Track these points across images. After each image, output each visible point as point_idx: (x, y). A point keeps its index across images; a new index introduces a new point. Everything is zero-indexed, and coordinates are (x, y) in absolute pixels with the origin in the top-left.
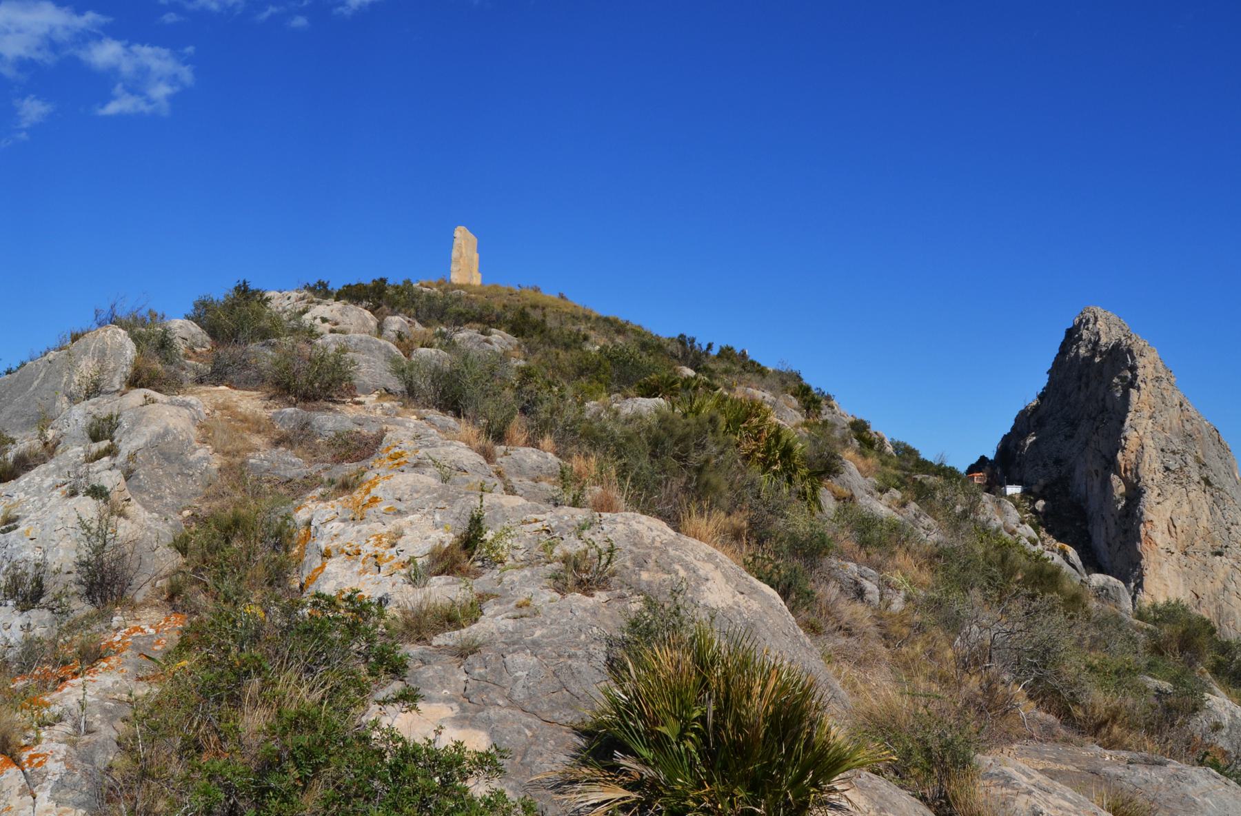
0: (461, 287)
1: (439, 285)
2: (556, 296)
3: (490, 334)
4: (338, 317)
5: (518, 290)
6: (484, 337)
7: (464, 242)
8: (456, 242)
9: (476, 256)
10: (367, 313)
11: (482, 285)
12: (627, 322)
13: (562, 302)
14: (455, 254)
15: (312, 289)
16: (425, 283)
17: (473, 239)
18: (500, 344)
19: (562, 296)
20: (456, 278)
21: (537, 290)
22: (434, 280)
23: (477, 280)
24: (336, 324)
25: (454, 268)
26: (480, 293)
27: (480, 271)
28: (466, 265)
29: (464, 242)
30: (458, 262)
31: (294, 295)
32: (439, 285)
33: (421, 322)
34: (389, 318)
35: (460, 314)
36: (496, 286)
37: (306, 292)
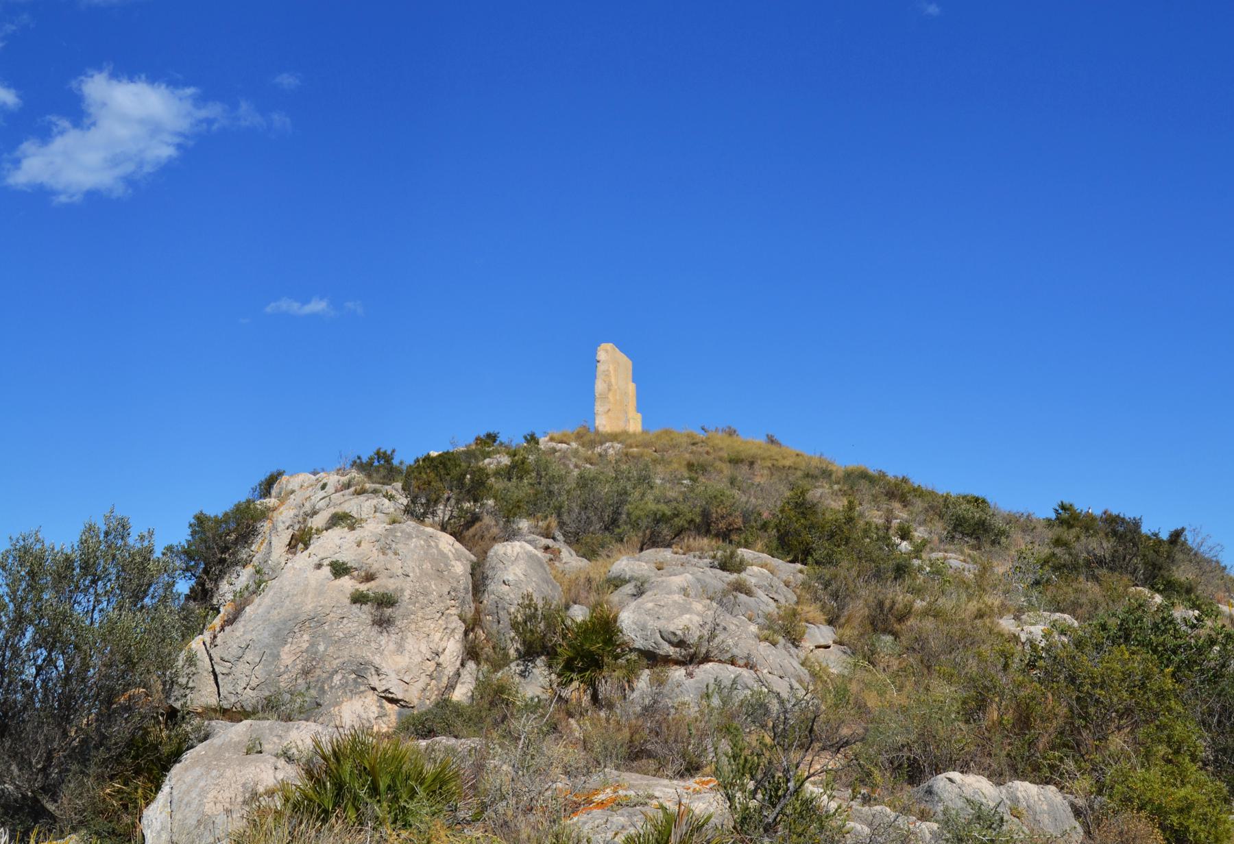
0: (613, 437)
1: (579, 437)
2: (761, 440)
3: (740, 567)
4: (375, 560)
5: (702, 435)
6: (733, 577)
7: (613, 367)
8: (601, 368)
9: (632, 387)
10: (446, 542)
11: (644, 432)
12: (905, 480)
13: (774, 449)
14: (600, 386)
15: (365, 467)
16: (557, 435)
17: (625, 362)
18: (769, 589)
19: (771, 440)
20: (604, 423)
21: (731, 433)
22: (570, 429)
23: (635, 425)
24: (370, 578)
25: (599, 408)
26: (646, 445)
27: (638, 410)
28: (617, 401)
29: (613, 367)
30: (605, 398)
31: (333, 479)
32: (579, 437)
33: (574, 539)
34: (500, 549)
35: (659, 519)
36: (667, 432)
37: (354, 473)
